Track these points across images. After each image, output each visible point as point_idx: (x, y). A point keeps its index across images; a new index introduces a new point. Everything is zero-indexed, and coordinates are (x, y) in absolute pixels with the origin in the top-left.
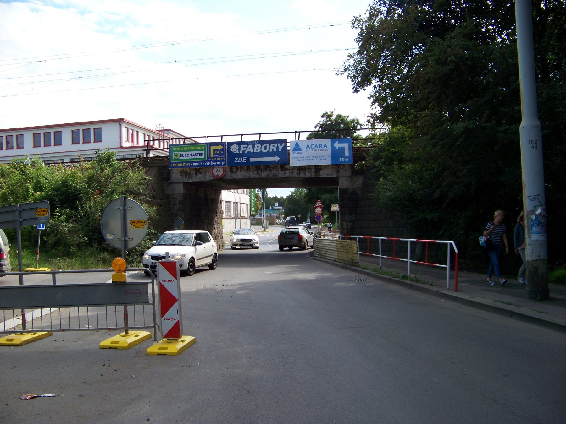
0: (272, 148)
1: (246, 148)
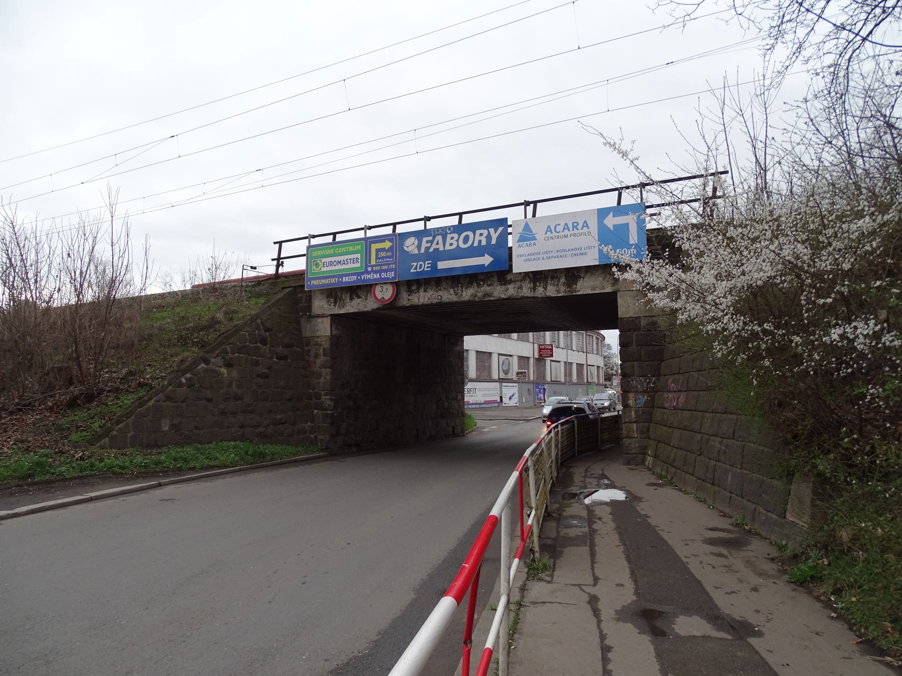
0: (478, 238)
1: (431, 242)
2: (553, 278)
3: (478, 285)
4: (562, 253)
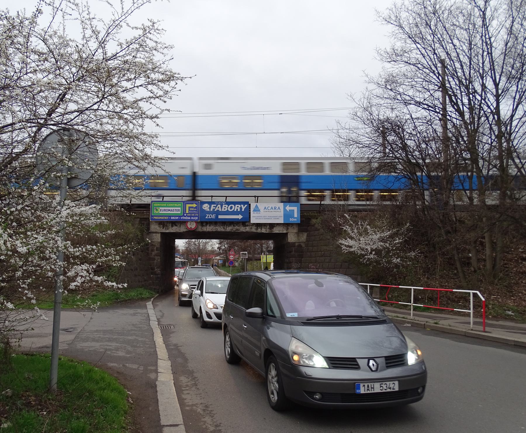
0: (236, 208)
1: (216, 207)
2: (264, 226)
3: (234, 226)
4: (270, 218)
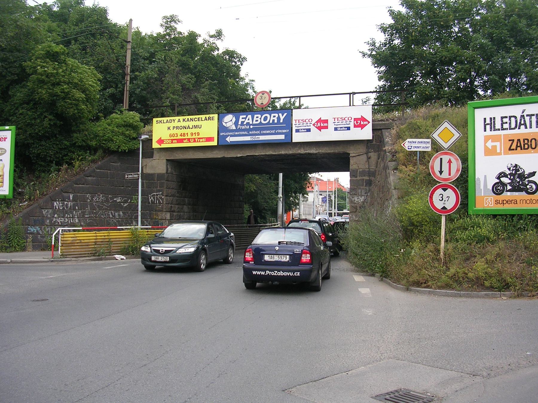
0: (272, 118)
1: (245, 118)
